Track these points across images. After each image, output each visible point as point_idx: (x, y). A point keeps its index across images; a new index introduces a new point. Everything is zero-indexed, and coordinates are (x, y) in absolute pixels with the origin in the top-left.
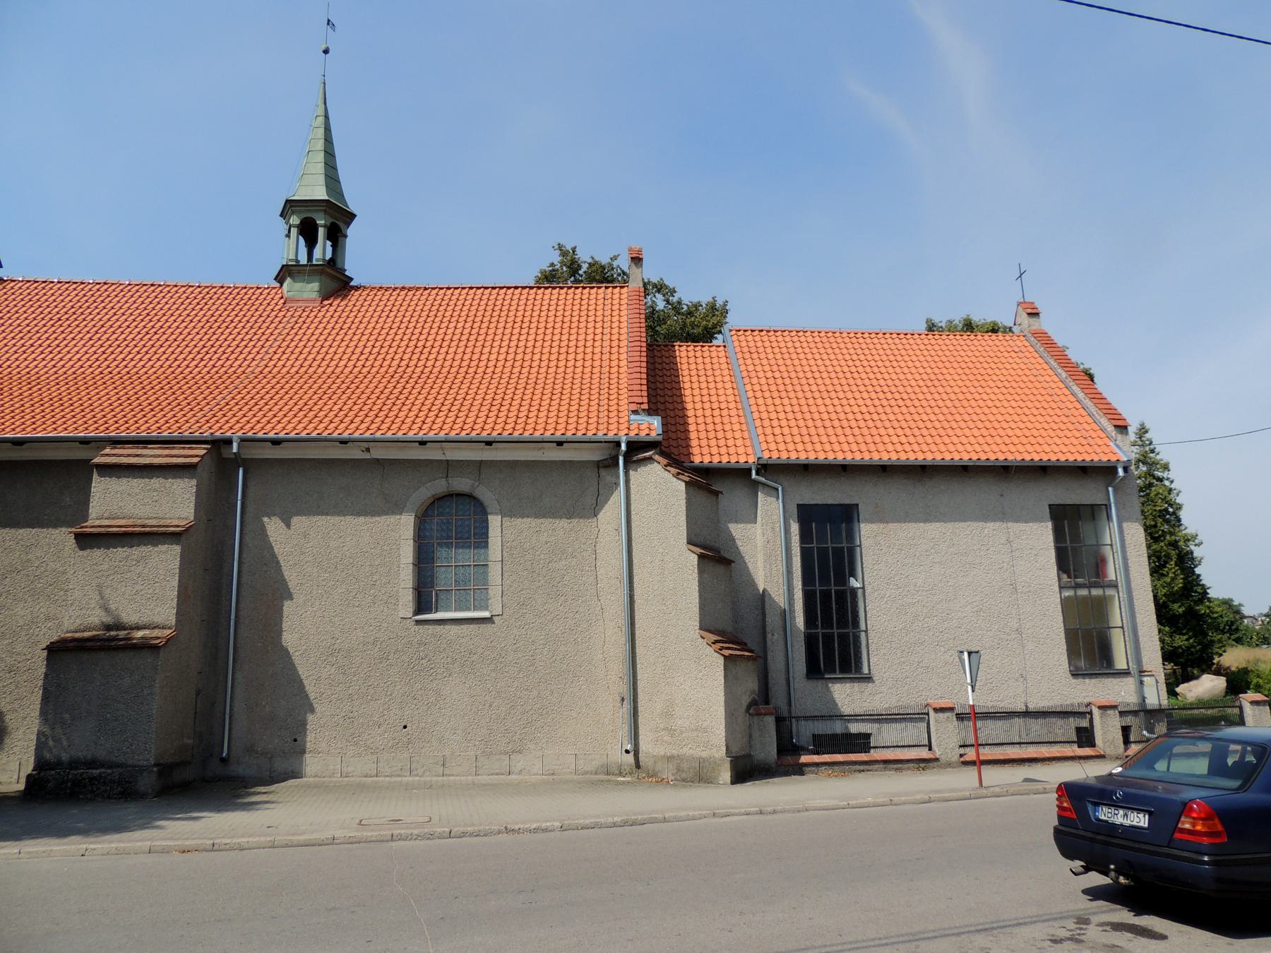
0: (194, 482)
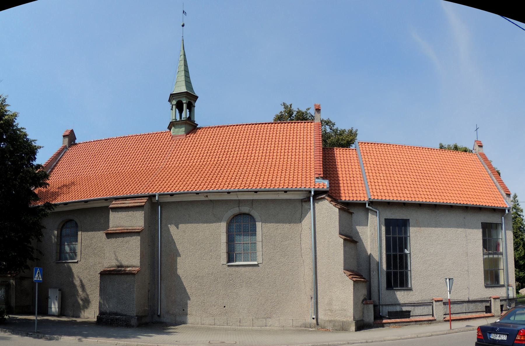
0: (143, 212)
